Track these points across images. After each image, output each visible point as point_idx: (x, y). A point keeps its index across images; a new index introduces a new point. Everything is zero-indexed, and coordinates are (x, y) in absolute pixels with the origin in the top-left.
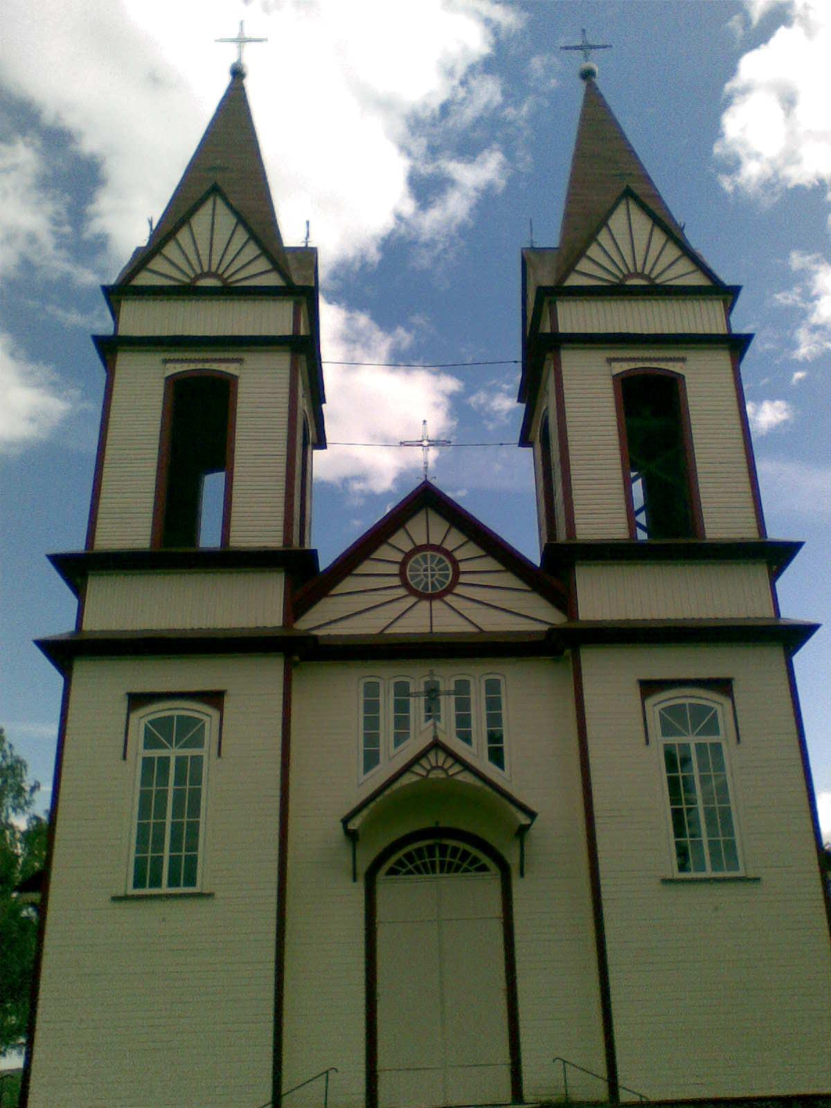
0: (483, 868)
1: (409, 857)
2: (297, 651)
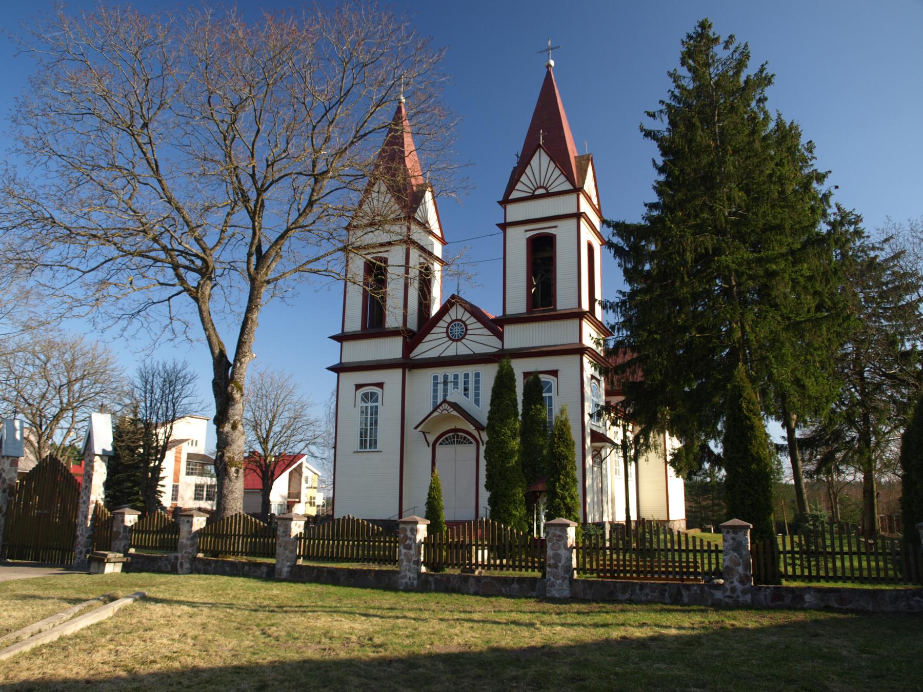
0: (471, 443)
1: (446, 439)
2: (407, 364)
